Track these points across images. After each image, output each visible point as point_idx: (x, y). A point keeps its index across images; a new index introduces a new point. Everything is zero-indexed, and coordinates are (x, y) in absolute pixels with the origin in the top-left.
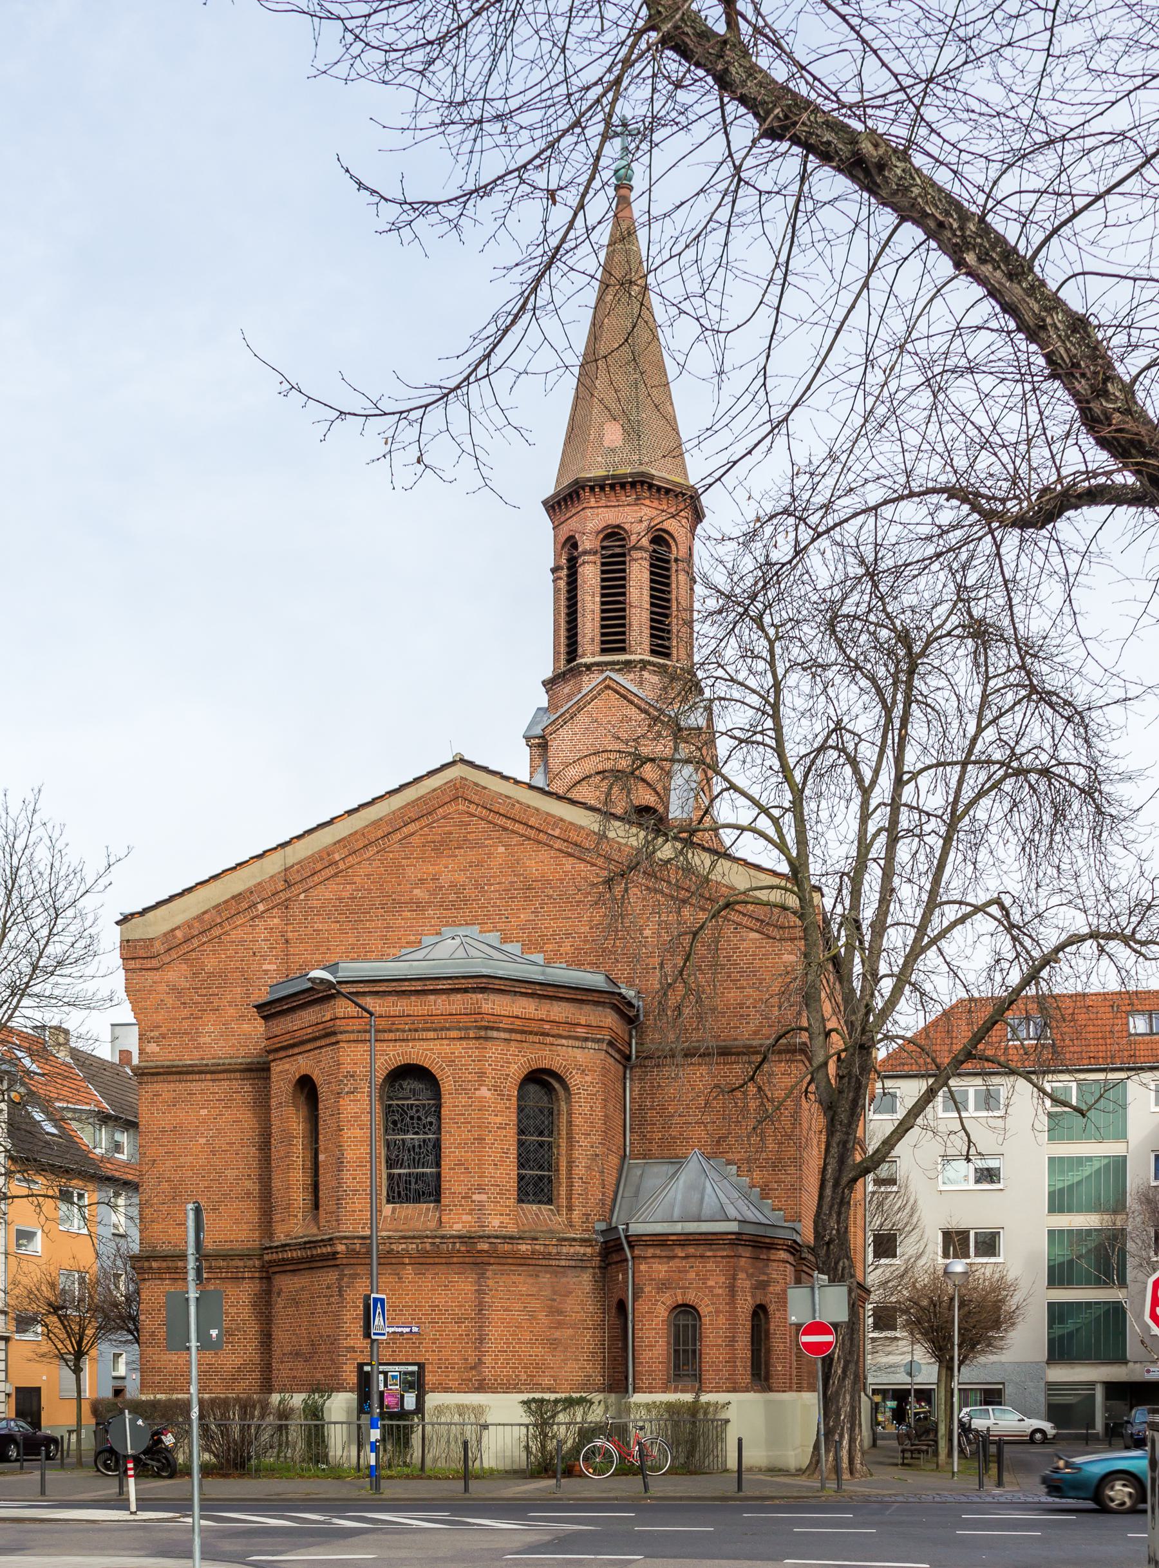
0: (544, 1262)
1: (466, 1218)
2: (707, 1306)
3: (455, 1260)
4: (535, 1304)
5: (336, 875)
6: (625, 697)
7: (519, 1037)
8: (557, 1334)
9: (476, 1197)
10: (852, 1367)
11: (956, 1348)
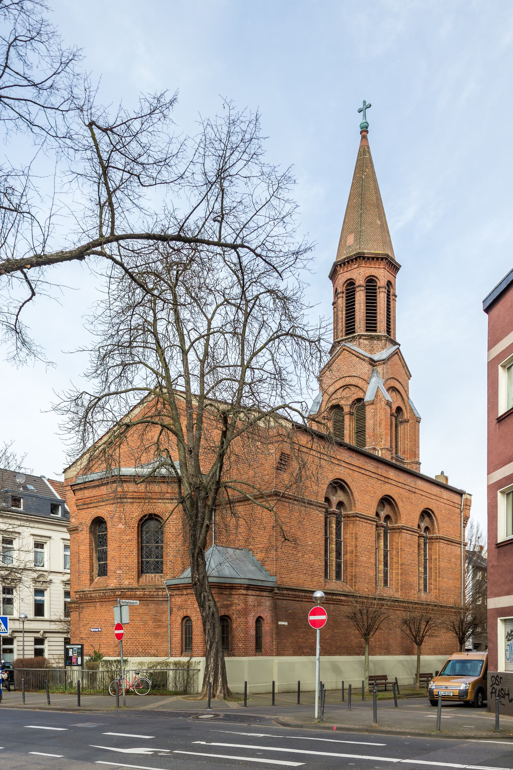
0: (150, 599)
1: (115, 581)
3: (111, 599)
4: (146, 618)
6: (350, 352)
7: (137, 501)
8: (158, 631)
9: (118, 572)
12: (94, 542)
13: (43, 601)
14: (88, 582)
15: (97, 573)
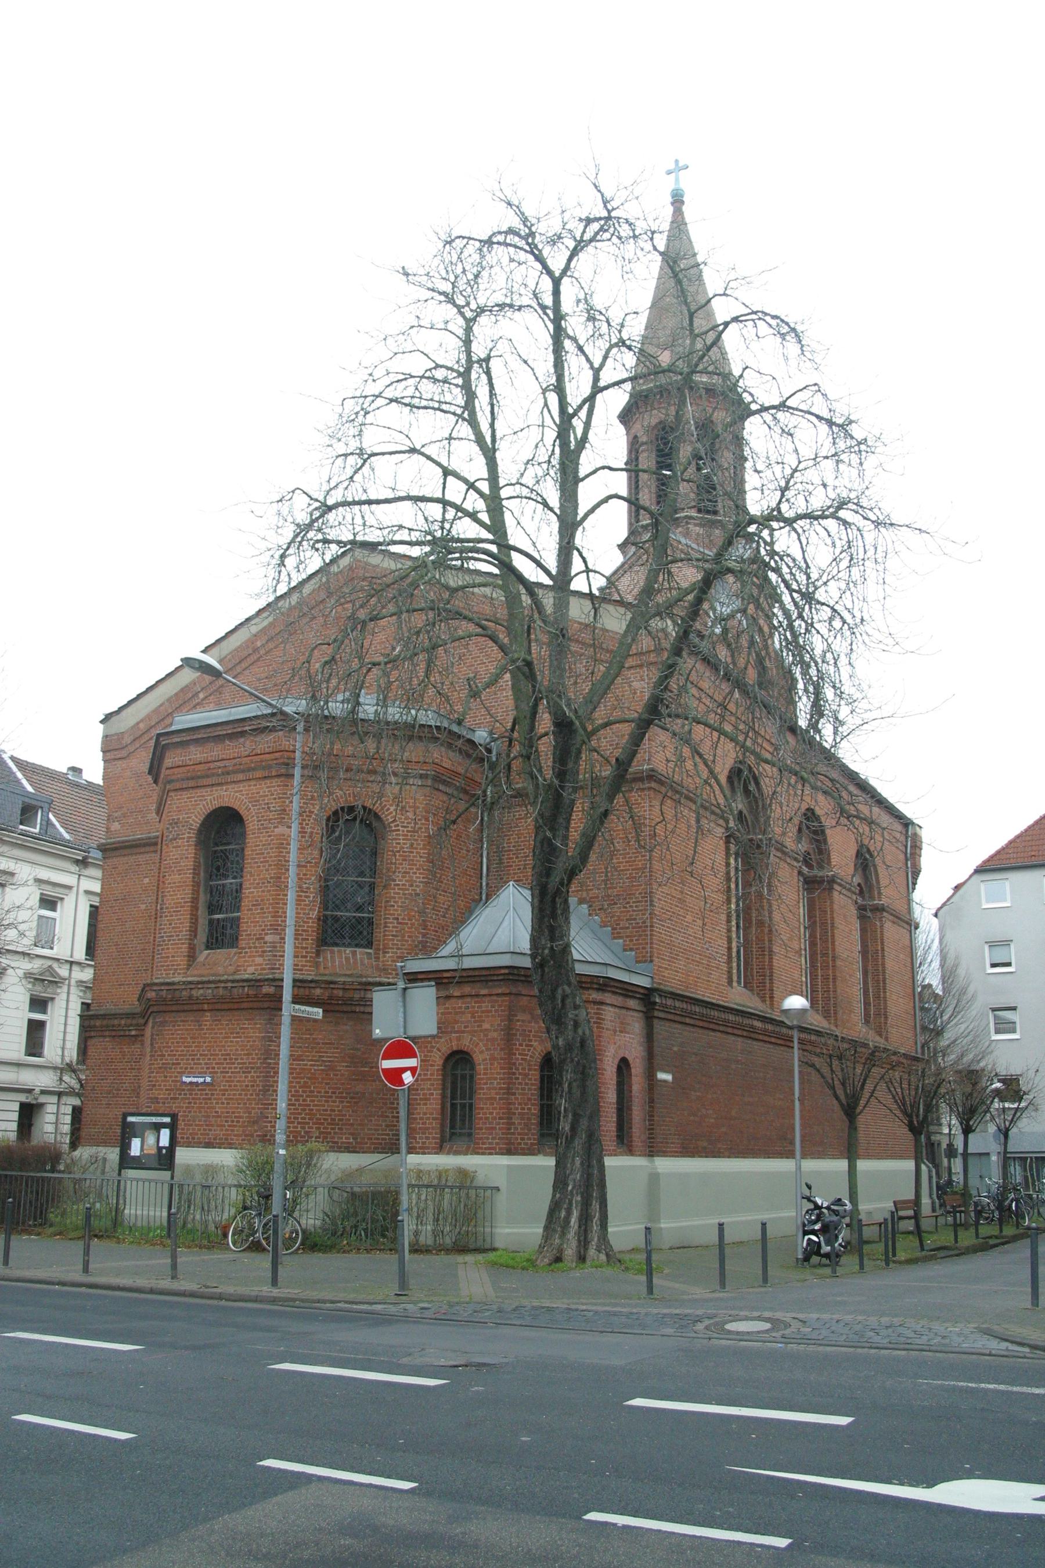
2: (482, 1052)
5: (258, 660)
8: (359, 1088)
10: (584, 1123)
11: (797, 1103)
12: (202, 868)
13: (30, 1011)
14: (182, 961)
15: (205, 940)
